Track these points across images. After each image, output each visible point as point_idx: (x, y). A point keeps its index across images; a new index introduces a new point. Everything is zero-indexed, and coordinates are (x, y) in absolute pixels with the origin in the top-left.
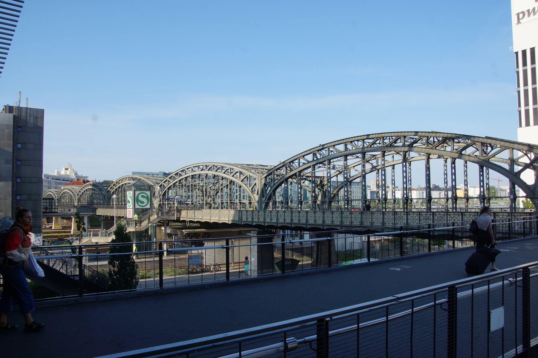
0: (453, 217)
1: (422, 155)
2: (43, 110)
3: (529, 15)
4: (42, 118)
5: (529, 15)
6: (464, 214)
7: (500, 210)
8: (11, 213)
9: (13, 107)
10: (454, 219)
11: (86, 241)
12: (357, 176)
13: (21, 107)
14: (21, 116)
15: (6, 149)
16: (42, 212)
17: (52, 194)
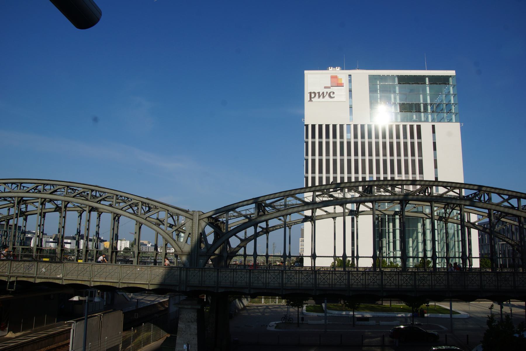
0: (306, 276)
1: (77, 206)
3: (319, 97)
5: (319, 97)
6: (252, 271)
7: (310, 269)
10: (374, 281)
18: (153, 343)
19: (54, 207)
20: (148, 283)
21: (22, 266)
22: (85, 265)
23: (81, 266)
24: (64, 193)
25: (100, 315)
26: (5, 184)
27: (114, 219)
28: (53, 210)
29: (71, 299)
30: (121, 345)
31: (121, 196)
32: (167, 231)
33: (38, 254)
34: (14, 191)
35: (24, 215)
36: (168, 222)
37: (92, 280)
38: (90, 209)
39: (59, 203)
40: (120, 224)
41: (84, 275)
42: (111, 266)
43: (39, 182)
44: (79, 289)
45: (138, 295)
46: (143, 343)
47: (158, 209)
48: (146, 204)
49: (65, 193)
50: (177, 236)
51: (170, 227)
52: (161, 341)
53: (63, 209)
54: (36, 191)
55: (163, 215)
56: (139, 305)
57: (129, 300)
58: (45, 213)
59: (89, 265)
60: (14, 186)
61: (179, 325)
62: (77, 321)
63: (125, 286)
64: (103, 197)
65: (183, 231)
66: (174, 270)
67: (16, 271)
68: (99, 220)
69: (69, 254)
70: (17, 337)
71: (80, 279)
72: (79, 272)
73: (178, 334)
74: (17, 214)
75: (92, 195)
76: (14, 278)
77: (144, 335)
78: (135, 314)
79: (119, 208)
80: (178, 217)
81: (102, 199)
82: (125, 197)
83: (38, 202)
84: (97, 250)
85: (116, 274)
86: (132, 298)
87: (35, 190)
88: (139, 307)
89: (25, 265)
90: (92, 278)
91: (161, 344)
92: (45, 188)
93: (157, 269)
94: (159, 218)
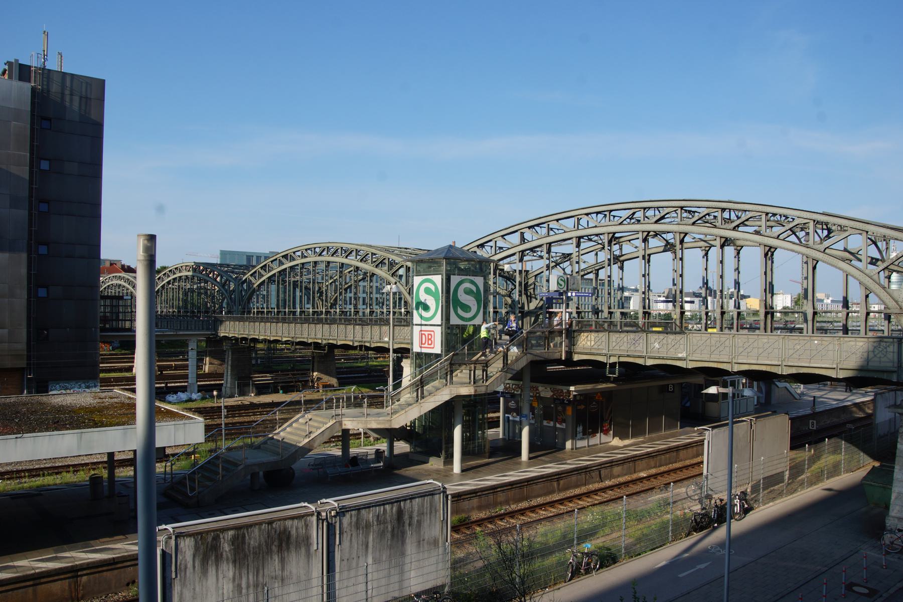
2: (104, 81)
4: (101, 99)
8: (25, 330)
9: (30, 67)
11: (328, 425)
12: (586, 272)
13: (49, 70)
14: (49, 91)
15: (14, 170)
16: (99, 330)
17: (126, 285)
18: (846, 475)
19: (663, 243)
20: (835, 366)
21: (625, 339)
22: (722, 336)
23: (715, 339)
24: (676, 220)
25: (751, 420)
26: (587, 214)
27: (766, 255)
28: (662, 249)
29: (705, 391)
30: (787, 473)
31: (774, 215)
32: (867, 272)
33: (646, 321)
34: (600, 225)
35: (618, 260)
36: (868, 255)
37: (734, 361)
38: (722, 243)
39: (669, 237)
40: (774, 265)
41: (750, 354)
42: (766, 337)
43: (637, 207)
44: (714, 375)
45: (814, 389)
46: (828, 473)
47: (845, 231)
48: (822, 225)
49: (679, 219)
50: (887, 280)
51: (871, 263)
52: (860, 474)
53: (678, 246)
54: (633, 221)
55: (856, 242)
56: (816, 407)
57: (797, 397)
58: (649, 255)
59: (728, 336)
60: (600, 216)
61: (899, 446)
62: (713, 428)
63: (793, 371)
64: (743, 218)
65: (898, 270)
66: (886, 342)
67: (617, 347)
68: (739, 261)
69: (690, 321)
70: (625, 446)
71: (715, 360)
72: (713, 348)
73: (896, 462)
74: (609, 260)
75: (723, 219)
76: (615, 357)
77: (828, 459)
78: (811, 421)
79: (772, 236)
80: (887, 243)
81: (740, 224)
82: (780, 215)
83: (638, 238)
84: (739, 310)
85: (776, 351)
86: (802, 394)
87: (631, 219)
88: (817, 410)
89: (629, 338)
90: (735, 357)
91: (862, 478)
92: (647, 214)
93: (852, 341)
94: (849, 248)
